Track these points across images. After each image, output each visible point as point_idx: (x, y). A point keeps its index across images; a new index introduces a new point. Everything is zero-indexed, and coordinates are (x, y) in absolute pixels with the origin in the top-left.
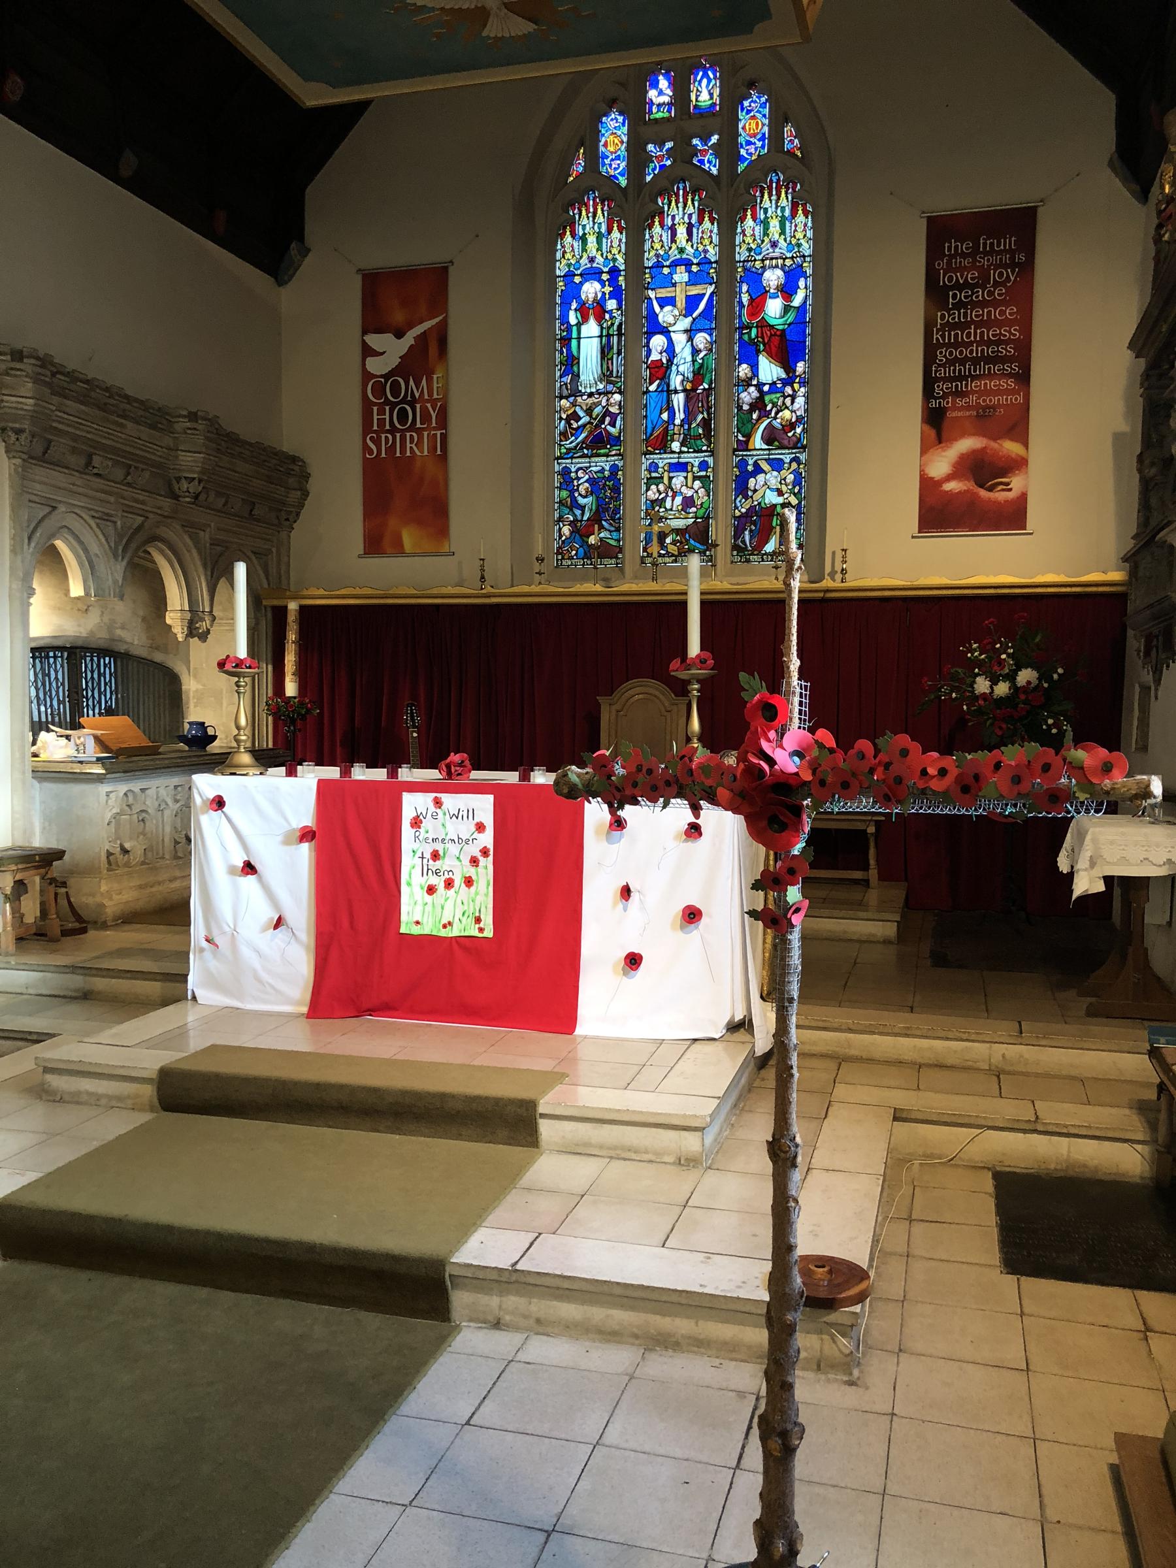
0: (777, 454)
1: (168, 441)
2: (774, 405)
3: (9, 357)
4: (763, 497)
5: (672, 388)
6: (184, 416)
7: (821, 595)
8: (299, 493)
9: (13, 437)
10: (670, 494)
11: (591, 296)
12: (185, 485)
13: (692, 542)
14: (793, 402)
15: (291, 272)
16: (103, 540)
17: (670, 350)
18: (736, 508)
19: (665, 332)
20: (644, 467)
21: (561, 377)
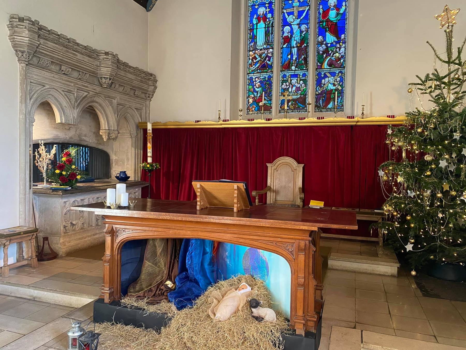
0: (333, 70)
1: (97, 63)
2: (332, 51)
3: (17, 20)
4: (328, 86)
5: (292, 46)
6: (103, 53)
7: (355, 123)
8: (153, 87)
9: (20, 54)
10: (291, 86)
11: (262, 13)
12: (104, 80)
13: (299, 104)
14: (340, 50)
15: (151, 6)
16: (68, 100)
17: (292, 32)
18: (316, 91)
19: (290, 25)
20: (281, 76)
21: (250, 43)
